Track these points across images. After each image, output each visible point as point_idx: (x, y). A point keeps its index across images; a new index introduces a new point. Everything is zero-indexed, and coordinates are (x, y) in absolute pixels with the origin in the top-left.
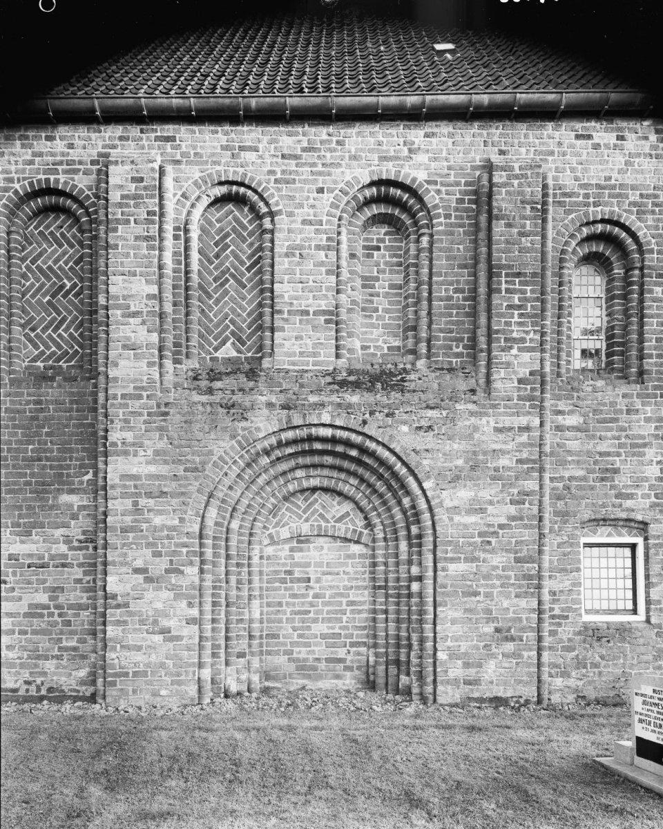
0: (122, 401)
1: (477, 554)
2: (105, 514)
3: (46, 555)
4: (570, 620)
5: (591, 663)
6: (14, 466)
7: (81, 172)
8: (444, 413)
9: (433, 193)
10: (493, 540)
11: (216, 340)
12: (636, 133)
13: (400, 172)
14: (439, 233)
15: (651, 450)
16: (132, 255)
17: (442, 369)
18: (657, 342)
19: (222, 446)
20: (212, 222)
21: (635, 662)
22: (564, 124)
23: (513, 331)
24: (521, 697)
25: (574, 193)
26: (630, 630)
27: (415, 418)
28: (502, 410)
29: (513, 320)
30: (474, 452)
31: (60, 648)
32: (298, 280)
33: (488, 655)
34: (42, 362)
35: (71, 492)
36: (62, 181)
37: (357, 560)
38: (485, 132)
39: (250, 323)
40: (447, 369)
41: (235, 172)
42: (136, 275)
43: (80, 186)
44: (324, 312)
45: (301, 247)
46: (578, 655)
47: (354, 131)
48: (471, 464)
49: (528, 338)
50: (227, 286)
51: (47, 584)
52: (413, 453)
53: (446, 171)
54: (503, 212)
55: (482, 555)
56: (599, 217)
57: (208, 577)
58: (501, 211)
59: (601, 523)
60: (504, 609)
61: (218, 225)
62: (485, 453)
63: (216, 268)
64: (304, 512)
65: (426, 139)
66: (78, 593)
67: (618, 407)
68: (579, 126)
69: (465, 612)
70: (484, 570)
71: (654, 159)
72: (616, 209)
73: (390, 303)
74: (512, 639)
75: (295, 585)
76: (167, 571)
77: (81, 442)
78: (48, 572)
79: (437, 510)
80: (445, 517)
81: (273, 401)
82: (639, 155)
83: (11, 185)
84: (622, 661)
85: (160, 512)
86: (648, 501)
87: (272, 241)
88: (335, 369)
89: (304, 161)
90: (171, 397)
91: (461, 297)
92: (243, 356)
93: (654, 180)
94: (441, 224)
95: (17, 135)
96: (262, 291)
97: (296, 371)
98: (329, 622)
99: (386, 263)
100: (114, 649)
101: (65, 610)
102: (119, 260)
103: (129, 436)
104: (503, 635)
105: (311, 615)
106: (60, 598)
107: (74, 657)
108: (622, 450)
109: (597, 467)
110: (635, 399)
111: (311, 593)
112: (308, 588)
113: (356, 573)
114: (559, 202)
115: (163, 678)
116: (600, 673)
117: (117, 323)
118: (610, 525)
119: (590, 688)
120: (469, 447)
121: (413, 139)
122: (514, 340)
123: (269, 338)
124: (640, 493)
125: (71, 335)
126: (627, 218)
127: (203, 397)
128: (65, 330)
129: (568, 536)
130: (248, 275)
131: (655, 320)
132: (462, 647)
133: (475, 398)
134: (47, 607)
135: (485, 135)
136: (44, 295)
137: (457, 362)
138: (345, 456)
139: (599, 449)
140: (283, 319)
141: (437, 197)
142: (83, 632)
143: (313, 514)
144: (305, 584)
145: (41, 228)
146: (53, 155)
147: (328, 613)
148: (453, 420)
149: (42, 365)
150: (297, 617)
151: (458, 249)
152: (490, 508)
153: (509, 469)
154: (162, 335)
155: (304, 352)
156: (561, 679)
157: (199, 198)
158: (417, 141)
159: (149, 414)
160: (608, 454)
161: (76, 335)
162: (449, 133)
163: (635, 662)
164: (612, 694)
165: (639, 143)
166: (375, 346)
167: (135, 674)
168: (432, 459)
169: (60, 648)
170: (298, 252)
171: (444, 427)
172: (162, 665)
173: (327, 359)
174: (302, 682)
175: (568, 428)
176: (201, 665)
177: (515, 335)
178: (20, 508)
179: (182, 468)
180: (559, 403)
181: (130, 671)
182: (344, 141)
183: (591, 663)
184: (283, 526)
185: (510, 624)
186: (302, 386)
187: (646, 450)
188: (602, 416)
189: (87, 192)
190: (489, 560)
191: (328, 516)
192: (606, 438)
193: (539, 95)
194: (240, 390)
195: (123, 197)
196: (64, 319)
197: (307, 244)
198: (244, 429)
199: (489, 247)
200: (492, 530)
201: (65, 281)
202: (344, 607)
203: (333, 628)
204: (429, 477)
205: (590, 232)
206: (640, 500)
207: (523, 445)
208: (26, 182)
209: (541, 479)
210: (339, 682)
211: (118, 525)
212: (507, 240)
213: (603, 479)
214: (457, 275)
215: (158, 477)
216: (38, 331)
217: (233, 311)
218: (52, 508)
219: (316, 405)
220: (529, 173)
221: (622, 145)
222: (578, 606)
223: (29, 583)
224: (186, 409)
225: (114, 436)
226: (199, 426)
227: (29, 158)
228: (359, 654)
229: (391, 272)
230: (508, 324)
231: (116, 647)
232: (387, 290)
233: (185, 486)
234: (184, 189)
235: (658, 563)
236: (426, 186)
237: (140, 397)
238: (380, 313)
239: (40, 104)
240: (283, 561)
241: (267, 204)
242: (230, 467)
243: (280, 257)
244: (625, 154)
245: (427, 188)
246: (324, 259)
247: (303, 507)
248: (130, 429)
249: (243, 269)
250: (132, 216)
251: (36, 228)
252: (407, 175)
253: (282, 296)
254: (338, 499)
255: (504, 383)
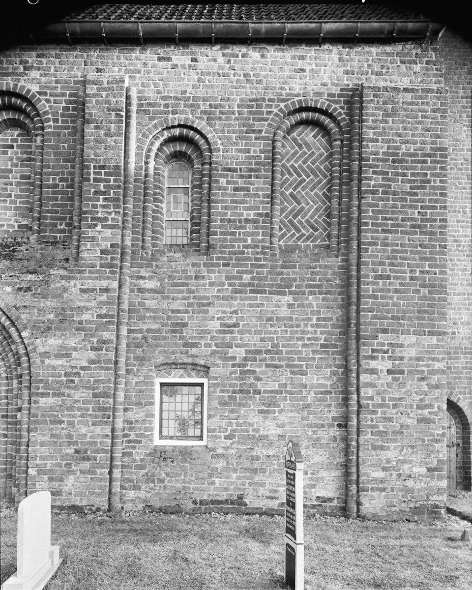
1: (62, 390)
4: (143, 444)
5: (158, 479)
8: (41, 277)
9: (43, 102)
10: (76, 379)
12: (207, 56)
13: (17, 85)
14: (48, 133)
15: (214, 309)
17: (48, 242)
18: (221, 222)
21: (193, 478)
22: (149, 49)
23: (99, 212)
24: (93, 506)
25: (157, 103)
26: (190, 453)
27: (18, 281)
28: (87, 275)
29: (99, 203)
30: (63, 308)
33: (68, 471)
38: (85, 54)
40: (51, 242)
46: (148, 472)
48: (60, 318)
49: (110, 217)
52: (14, 309)
53: (54, 85)
54: (93, 117)
55: (67, 392)
56: (176, 123)
58: (92, 116)
59: (173, 366)
60: (83, 435)
62: (72, 309)
65: (38, 59)
67: (189, 274)
68: (161, 51)
69: (51, 437)
70: (68, 403)
71: (222, 77)
72: (191, 116)
73: (21, 190)
74: (88, 459)
79: (31, 355)
80: (38, 360)
82: (209, 74)
84: (183, 477)
86: (209, 349)
91: (65, 185)
93: (221, 94)
94: (50, 127)
99: (18, 159)
104: (81, 455)
108: (190, 309)
109: (170, 322)
110: (202, 268)
114: (144, 110)
116: (165, 487)
118: (180, 368)
119: (157, 499)
120: (59, 305)
121: (27, 59)
122: (99, 219)
124: (203, 343)
126: (199, 123)
129: (144, 376)
131: (220, 205)
132: (48, 465)
133: (66, 265)
135: (85, 57)
137: (60, 237)
139: (172, 307)
141: (47, 105)
148: (47, 283)
151: (64, 146)
152: (74, 353)
153: (91, 322)
156: (133, 492)
158: (30, 60)
160: (179, 311)
162: (56, 54)
163: (193, 478)
164: (173, 504)
165: (209, 64)
166: (7, 225)
168: (29, 313)
171: (40, 288)
175: (148, 290)
177: (100, 215)
180: (141, 270)
183: (158, 479)
185: (87, 447)
187: (210, 308)
188: (175, 281)
190: (72, 395)
192: (178, 298)
193: (119, 24)
200: (75, 371)
204: (25, 328)
205: (170, 135)
206: (203, 348)
207: (103, 303)
209: (118, 330)
212: (95, 139)
213: (173, 332)
214: (62, 167)
220: (115, 86)
221: (195, 65)
222: (150, 433)
229: (22, 165)
230: (95, 206)
232: (18, 180)
235: (216, 399)
236: (38, 96)
238: (13, 198)
239: (58, 27)
244: (198, 73)
245: (39, 98)
252: (23, 87)
255: (90, 254)
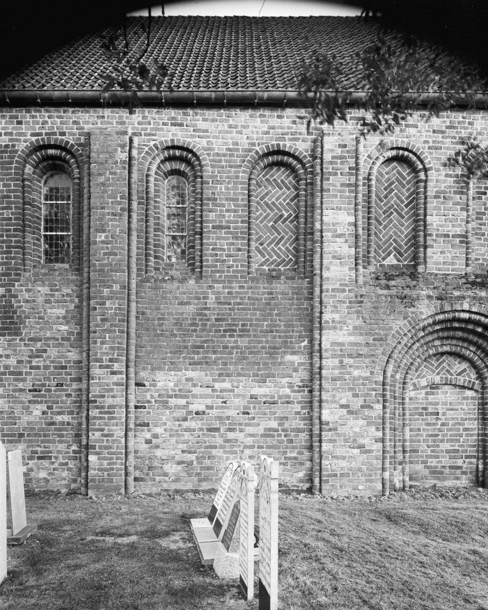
0: (333, 293)
2: (320, 368)
3: (276, 395)
6: (254, 336)
7: (301, 140)
11: (384, 253)
16: (339, 196)
19: (398, 324)
20: (383, 174)
31: (285, 458)
32: (442, 214)
34: (267, 266)
35: (294, 353)
36: (288, 145)
37: (470, 401)
39: (407, 242)
41: (402, 141)
42: (341, 210)
43: (300, 149)
44: (459, 236)
45: (445, 192)
47: (480, 116)
50: (392, 217)
51: (277, 415)
57: (388, 411)
61: (387, 176)
63: (385, 205)
64: (436, 368)
66: (297, 421)
75: (429, 417)
76: (362, 407)
77: (300, 320)
78: (277, 407)
81: (431, 294)
83: (253, 147)
85: (358, 368)
87: (425, 187)
88: (466, 274)
89: (447, 135)
90: (363, 291)
92: (401, 264)
95: (258, 114)
96: (416, 221)
97: (441, 275)
98: (452, 442)
100: (327, 458)
101: (289, 432)
102: (330, 199)
103: (337, 317)
105: (440, 437)
106: (285, 424)
107: (295, 464)
111: (440, 422)
112: (437, 419)
113: (469, 409)
115: (360, 478)
117: (329, 241)
123: (423, 253)
125: (287, 248)
127: (384, 291)
128: (283, 245)
130: (406, 210)
134: (277, 430)
136: (269, 221)
138: (473, 332)
140: (432, 239)
142: (301, 447)
143: (442, 369)
144: (435, 417)
145: (267, 177)
146: (282, 128)
147: (451, 435)
149: (267, 268)
150: (430, 438)
154: (357, 250)
155: (446, 262)
157: (377, 158)
159: (350, 302)
161: (291, 248)
166: (483, 259)
167: (342, 475)
169: (285, 458)
170: (442, 195)
172: (360, 470)
173: (460, 267)
174: (433, 482)
176: (383, 469)
178: (258, 364)
179: (372, 338)
181: (338, 473)
182: (473, 122)
184: (423, 377)
186: (447, 284)
189: (305, 154)
191: (452, 371)
194: (407, 287)
195: (333, 157)
196: (282, 238)
197: (448, 190)
198: (413, 313)
201: (284, 212)
202: (461, 432)
203: (453, 446)
208: (264, 146)
210: (458, 482)
211: (330, 376)
215: (356, 344)
216: (265, 245)
217: (396, 233)
218: (280, 364)
219: (459, 297)
223: (265, 414)
224: (374, 299)
225: (327, 317)
226: (382, 310)
227: (266, 129)
228: (471, 463)
231: (329, 457)
233: (374, 350)
234: (369, 152)
237: (344, 291)
240: (421, 401)
241: (422, 162)
242: (402, 338)
243: (431, 198)
246: (459, 200)
247: (436, 365)
248: (338, 312)
249: (403, 206)
250: (339, 170)
251: (264, 176)
253: (432, 224)
254: (458, 360)
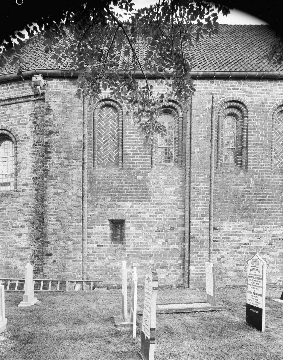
34: (279, 165)
145: (279, 117)
149: (279, 166)
199: (9, 104)
208: (280, 101)
223: (280, 245)
